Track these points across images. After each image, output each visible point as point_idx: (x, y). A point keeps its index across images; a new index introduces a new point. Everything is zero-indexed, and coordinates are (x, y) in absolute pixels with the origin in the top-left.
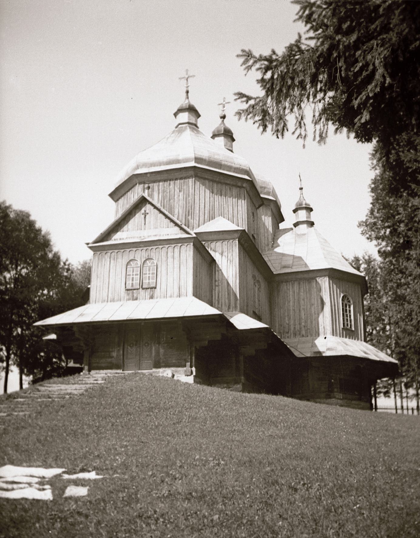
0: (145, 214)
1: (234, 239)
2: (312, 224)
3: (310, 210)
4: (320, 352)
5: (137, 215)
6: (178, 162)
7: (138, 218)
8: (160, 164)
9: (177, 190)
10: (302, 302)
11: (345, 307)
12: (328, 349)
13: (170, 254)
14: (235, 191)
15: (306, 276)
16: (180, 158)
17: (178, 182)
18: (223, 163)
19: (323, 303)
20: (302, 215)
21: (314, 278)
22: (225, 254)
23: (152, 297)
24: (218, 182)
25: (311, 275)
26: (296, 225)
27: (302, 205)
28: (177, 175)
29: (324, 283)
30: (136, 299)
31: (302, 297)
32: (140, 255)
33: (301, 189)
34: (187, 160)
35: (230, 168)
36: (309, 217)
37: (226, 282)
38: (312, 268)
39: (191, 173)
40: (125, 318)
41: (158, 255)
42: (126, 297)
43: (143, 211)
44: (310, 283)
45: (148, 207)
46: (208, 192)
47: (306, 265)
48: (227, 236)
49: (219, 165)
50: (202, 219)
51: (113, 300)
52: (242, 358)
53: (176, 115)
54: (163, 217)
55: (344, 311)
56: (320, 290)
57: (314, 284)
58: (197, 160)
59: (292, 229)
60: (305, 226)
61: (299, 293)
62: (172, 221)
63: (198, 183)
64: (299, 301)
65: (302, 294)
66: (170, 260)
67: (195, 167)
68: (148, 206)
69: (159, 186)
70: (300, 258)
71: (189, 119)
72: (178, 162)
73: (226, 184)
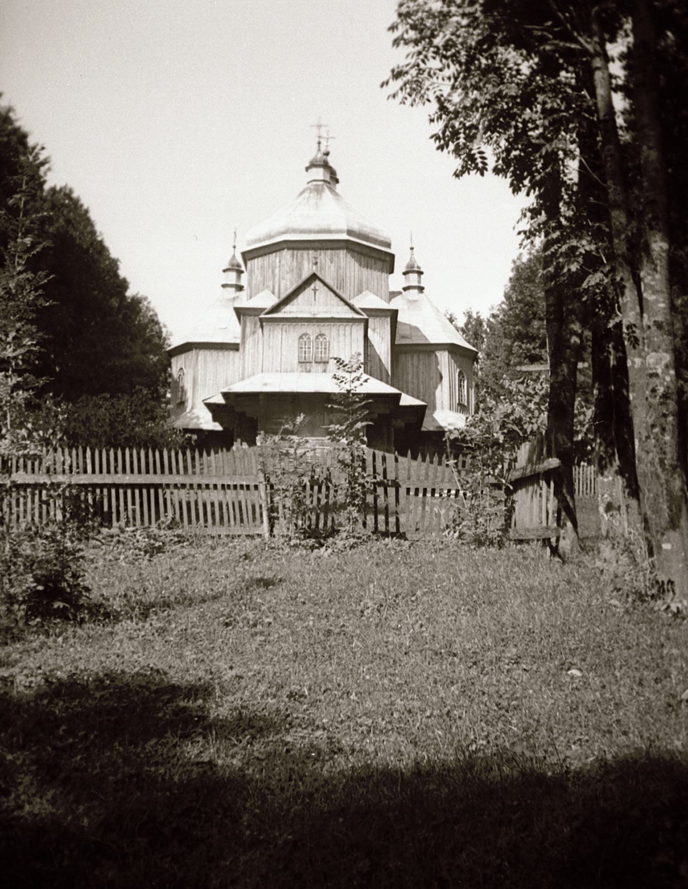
0: (315, 290)
1: (387, 317)
2: (421, 289)
3: (420, 273)
4: (441, 427)
5: (307, 290)
6: (329, 232)
7: (308, 292)
8: (310, 232)
9: (328, 261)
10: (421, 376)
11: (460, 381)
12: (449, 424)
13: (341, 332)
14: (379, 264)
15: (425, 348)
16: (333, 228)
17: (329, 252)
18: (371, 235)
19: (441, 377)
20: (413, 279)
21: (433, 352)
22: (378, 330)
23: (325, 371)
24: (365, 255)
25: (428, 348)
26: (405, 289)
27: (413, 267)
28: (329, 245)
29: (444, 358)
30: (309, 371)
31: (421, 371)
32: (312, 330)
33: (412, 249)
34: (339, 232)
35: (375, 241)
36: (419, 282)
37: (377, 361)
38: (432, 342)
39: (344, 244)
40: (312, 390)
41: (331, 332)
42: (300, 369)
43: (312, 286)
44: (429, 356)
45: (317, 284)
46: (357, 265)
47: (426, 339)
48: (379, 314)
49: (366, 238)
50: (352, 292)
51: (286, 371)
52: (392, 430)
53: (307, 169)
54: (333, 295)
55: (460, 386)
56: (437, 363)
57: (433, 357)
58: (350, 232)
59: (400, 293)
60: (416, 291)
61: (418, 367)
62: (342, 299)
63: (349, 256)
64: (418, 374)
65: (421, 367)
66: (342, 338)
67: (348, 241)
68: (318, 283)
69: (308, 254)
70: (417, 328)
71: (324, 176)
72: (329, 232)
73: (372, 257)
